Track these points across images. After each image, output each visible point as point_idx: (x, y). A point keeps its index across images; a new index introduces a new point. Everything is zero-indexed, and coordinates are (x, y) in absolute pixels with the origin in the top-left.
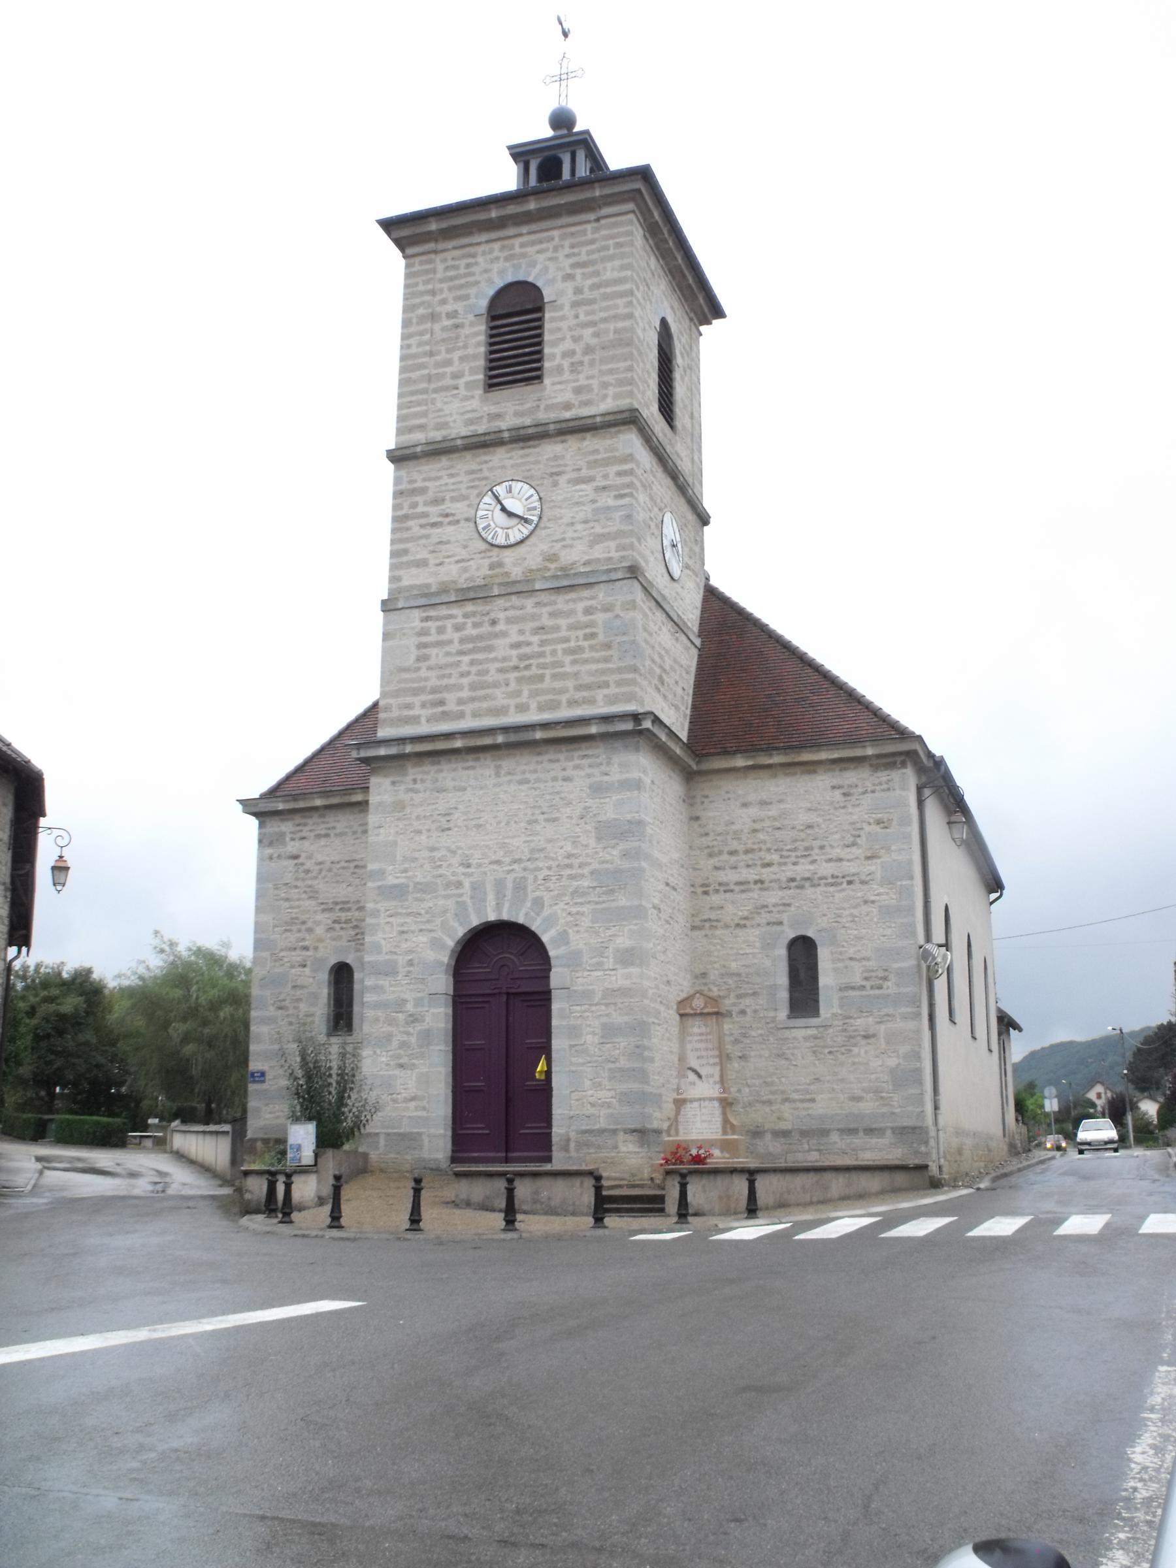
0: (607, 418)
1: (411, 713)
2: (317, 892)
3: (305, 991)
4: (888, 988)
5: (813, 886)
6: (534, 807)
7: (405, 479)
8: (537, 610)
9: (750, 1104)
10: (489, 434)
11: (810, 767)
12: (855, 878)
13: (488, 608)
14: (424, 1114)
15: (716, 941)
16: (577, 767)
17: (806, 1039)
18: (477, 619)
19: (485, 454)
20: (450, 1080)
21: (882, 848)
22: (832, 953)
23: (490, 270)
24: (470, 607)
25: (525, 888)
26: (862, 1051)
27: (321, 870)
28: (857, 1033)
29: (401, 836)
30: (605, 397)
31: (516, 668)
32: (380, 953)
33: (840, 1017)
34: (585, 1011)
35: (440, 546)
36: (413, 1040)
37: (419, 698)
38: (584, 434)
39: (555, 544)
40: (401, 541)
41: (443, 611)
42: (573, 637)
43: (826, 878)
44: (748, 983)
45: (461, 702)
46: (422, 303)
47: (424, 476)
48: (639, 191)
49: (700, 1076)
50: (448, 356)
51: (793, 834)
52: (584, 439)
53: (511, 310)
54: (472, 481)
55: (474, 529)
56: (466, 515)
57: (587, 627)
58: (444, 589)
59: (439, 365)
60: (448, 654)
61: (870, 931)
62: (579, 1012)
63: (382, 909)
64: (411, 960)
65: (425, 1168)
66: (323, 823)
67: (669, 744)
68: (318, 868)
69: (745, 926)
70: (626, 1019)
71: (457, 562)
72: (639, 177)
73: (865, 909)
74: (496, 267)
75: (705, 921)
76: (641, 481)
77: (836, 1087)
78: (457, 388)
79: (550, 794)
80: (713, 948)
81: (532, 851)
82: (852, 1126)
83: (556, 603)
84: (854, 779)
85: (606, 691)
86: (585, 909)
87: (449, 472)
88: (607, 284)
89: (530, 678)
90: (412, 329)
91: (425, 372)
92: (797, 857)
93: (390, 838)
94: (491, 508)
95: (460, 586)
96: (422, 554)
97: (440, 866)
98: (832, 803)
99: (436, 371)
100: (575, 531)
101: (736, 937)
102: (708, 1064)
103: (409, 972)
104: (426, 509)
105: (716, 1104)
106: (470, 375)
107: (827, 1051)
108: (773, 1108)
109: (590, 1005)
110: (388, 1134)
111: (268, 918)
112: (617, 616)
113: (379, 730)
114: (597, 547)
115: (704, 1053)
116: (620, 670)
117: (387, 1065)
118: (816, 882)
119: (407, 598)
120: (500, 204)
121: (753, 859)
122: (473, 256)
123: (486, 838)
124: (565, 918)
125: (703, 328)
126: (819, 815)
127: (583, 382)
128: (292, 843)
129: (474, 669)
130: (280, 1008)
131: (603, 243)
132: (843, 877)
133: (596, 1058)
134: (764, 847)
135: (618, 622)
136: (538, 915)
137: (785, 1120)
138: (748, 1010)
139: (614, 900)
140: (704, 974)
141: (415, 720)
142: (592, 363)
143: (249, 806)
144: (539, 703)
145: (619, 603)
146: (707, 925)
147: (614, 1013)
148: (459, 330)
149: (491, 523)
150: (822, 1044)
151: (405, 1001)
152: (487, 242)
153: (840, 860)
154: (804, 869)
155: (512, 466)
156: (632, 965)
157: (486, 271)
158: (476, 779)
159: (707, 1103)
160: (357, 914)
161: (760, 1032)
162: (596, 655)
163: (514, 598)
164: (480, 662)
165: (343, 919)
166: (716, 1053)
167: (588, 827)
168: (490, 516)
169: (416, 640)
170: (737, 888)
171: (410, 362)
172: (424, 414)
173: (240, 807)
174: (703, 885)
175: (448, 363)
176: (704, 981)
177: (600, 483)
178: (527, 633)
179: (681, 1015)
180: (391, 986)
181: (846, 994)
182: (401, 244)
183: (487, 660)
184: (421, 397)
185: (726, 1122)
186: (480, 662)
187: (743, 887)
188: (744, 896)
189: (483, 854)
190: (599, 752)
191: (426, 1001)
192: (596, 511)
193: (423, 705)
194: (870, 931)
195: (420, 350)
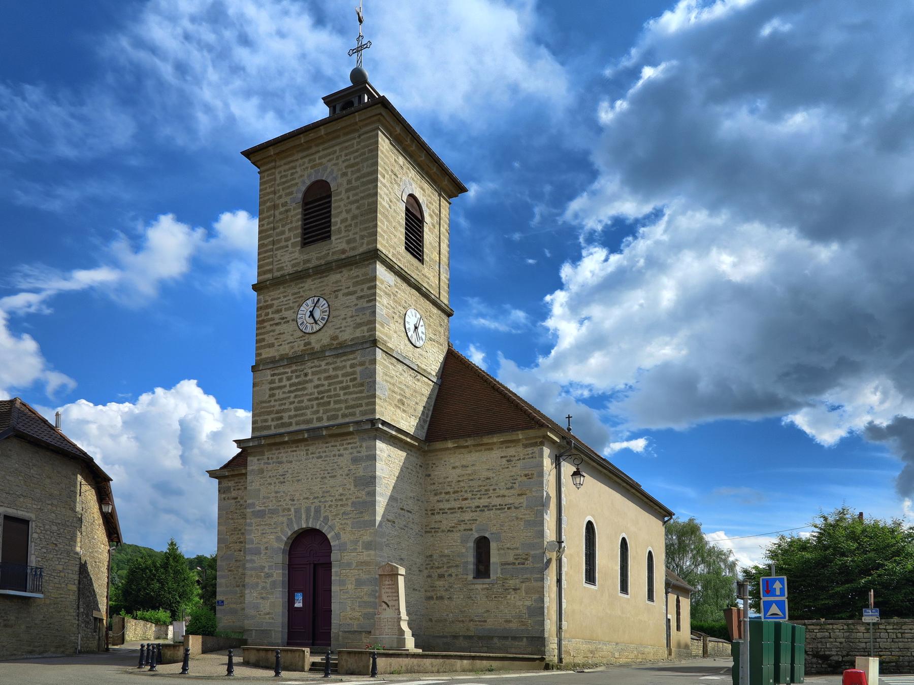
1: (267, 424)
3: (241, 563)
4: (528, 564)
13: (303, 367)
14: (273, 621)
16: (345, 449)
23: (304, 175)
26: (512, 597)
39: (336, 330)
42: (345, 380)
43: (496, 506)
45: (290, 417)
46: (268, 200)
48: (380, 114)
49: (388, 606)
50: (283, 229)
54: (295, 298)
56: (292, 318)
57: (352, 375)
58: (283, 358)
59: (278, 234)
60: (284, 393)
69: (452, 531)
70: (367, 577)
71: (288, 343)
72: (380, 105)
74: (306, 173)
83: (336, 362)
85: (361, 409)
86: (348, 522)
88: (364, 176)
89: (324, 403)
90: (264, 215)
96: (272, 340)
99: (277, 238)
100: (346, 322)
103: (266, 553)
109: (351, 570)
110: (256, 630)
112: (367, 368)
118: (491, 507)
119: (264, 364)
122: (294, 168)
129: (296, 400)
132: (505, 505)
134: (464, 490)
144: (328, 416)
146: (433, 530)
149: (305, 321)
152: (301, 158)
153: (504, 496)
154: (484, 501)
155: (315, 289)
162: (355, 389)
170: (449, 511)
171: (264, 234)
172: (272, 263)
174: (431, 510)
175: (283, 233)
177: (360, 294)
181: (504, 567)
184: (269, 254)
187: (452, 511)
191: (274, 567)
193: (273, 420)
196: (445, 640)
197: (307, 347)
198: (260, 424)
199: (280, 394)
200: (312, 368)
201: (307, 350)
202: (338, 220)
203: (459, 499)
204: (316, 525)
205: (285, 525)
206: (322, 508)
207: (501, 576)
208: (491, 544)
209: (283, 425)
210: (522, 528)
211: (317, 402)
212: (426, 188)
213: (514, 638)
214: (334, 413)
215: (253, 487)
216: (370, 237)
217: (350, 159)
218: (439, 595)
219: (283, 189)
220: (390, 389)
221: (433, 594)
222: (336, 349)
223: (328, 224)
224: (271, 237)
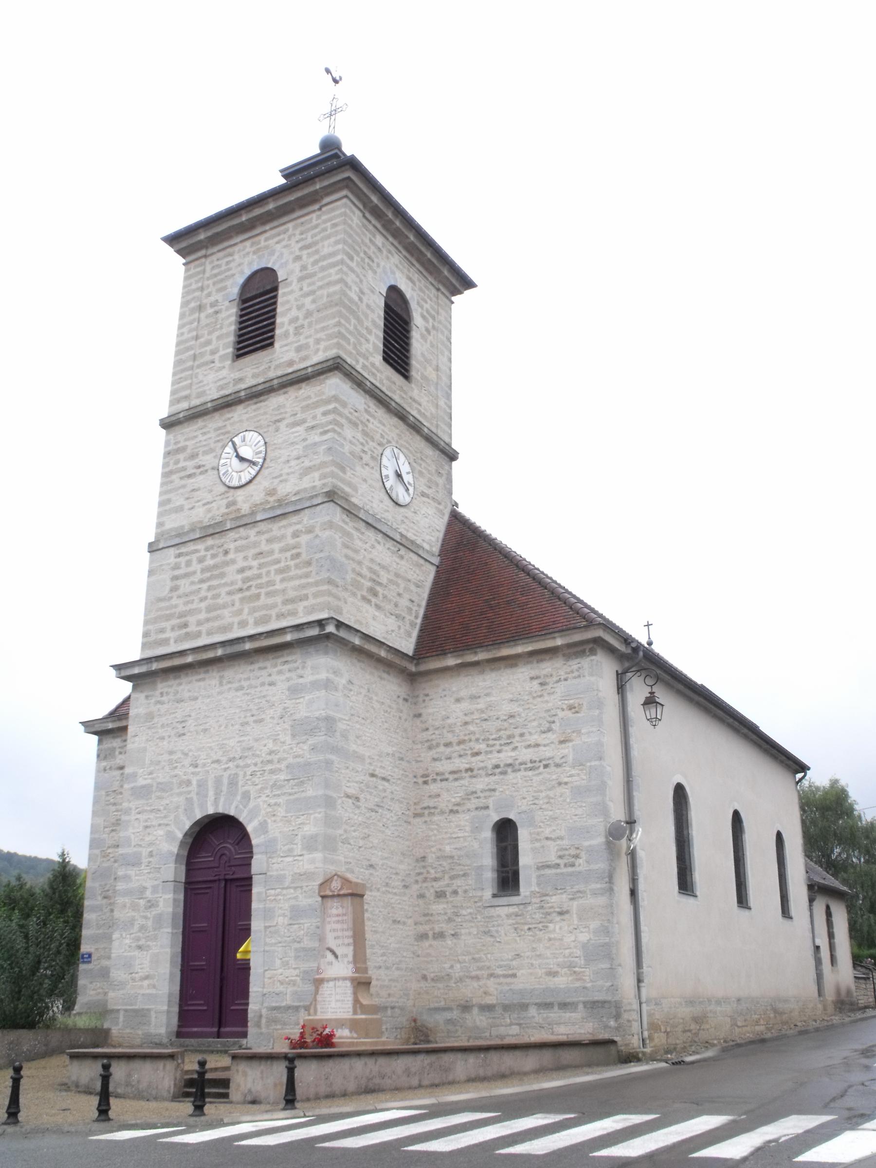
4: (580, 865)
5: (514, 771)
6: (246, 710)
7: (173, 442)
9: (461, 980)
11: (511, 661)
12: (550, 762)
13: (223, 540)
15: (433, 827)
16: (280, 672)
17: (508, 916)
19: (229, 412)
20: (179, 959)
21: (573, 732)
22: (531, 834)
24: (210, 542)
25: (237, 784)
26: (557, 927)
28: (552, 910)
29: (150, 743)
30: (318, 350)
33: (538, 895)
34: (278, 895)
35: (193, 493)
36: (150, 923)
41: (191, 547)
42: (283, 559)
44: (460, 865)
45: (199, 623)
48: (349, 178)
49: (336, 957)
50: (209, 337)
51: (498, 724)
52: (301, 388)
55: (217, 476)
56: (211, 466)
60: (193, 583)
61: (563, 811)
62: (273, 896)
63: (134, 807)
64: (151, 852)
65: (151, 1043)
67: (366, 647)
69: (457, 812)
71: (204, 505)
72: (348, 167)
73: (559, 790)
74: (247, 260)
75: (425, 808)
76: (347, 418)
77: (534, 962)
78: (213, 362)
79: (259, 698)
81: (244, 750)
82: (548, 1001)
83: (271, 530)
84: (550, 670)
85: (305, 603)
86: (280, 800)
88: (324, 258)
89: (250, 597)
91: (192, 352)
92: (501, 745)
94: (229, 456)
97: (176, 768)
98: (530, 693)
99: (200, 351)
100: (290, 467)
101: (450, 822)
102: (343, 944)
103: (150, 862)
108: (481, 983)
109: (283, 889)
110: (126, 1011)
111: (100, 821)
112: (317, 536)
115: (340, 934)
116: (317, 584)
117: (130, 947)
118: (517, 767)
120: (248, 209)
121: (465, 750)
122: (231, 255)
123: (210, 740)
125: (453, 298)
126: (520, 705)
127: (303, 341)
128: (120, 756)
129: (210, 594)
130: (105, 897)
132: (540, 761)
133: (286, 939)
134: (473, 738)
135: (317, 541)
136: (245, 807)
137: (491, 995)
138: (459, 890)
139: (303, 791)
140: (424, 857)
142: (310, 325)
143: (90, 726)
144: (255, 618)
145: (319, 524)
146: (426, 812)
147: (300, 896)
148: (219, 315)
149: (230, 469)
150: (522, 921)
151: (145, 888)
152: (242, 242)
153: (537, 745)
154: (507, 756)
155: (247, 419)
156: (316, 850)
161: (469, 911)
162: (299, 572)
163: (241, 530)
166: (350, 933)
168: (228, 463)
170: (451, 777)
173: (82, 728)
174: (423, 776)
175: (208, 342)
176: (423, 864)
178: (250, 559)
179: (323, 897)
180: (136, 875)
181: (542, 872)
182: (181, 252)
183: (219, 586)
185: (356, 1001)
187: (456, 776)
188: (457, 784)
190: (296, 658)
191: (160, 887)
193: (173, 629)
194: (563, 811)
196: (448, 1015)
198: (153, 638)
200: (235, 541)
201: (231, 513)
204: (230, 808)
206: (241, 778)
209: (188, 636)
211: (240, 595)
212: (416, 280)
213: (564, 1006)
215: (136, 745)
216: (329, 340)
217: (306, 239)
218: (437, 930)
219: (214, 284)
220: (354, 570)
222: (272, 508)
223: (271, 327)
224: (192, 349)
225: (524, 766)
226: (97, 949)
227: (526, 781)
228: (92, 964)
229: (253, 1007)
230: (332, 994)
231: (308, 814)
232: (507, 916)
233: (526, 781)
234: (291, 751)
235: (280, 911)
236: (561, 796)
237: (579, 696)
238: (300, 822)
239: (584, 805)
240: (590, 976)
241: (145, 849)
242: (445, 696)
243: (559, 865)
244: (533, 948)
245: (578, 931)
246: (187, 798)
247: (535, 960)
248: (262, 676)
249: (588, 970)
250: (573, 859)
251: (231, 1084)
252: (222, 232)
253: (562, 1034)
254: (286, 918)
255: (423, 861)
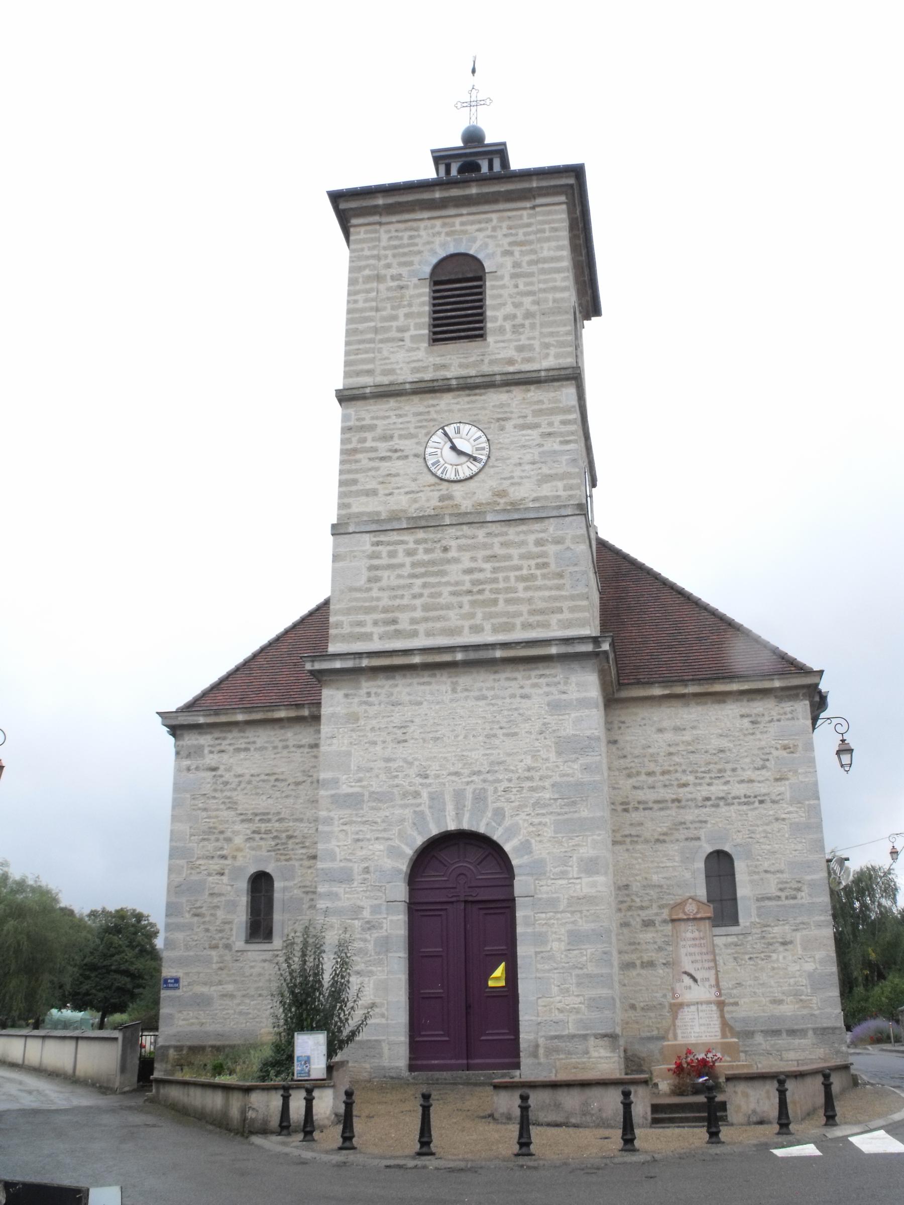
0: (551, 373)
1: (363, 630)
2: (236, 803)
3: (223, 898)
4: (802, 898)
6: (493, 722)
7: (353, 417)
8: (489, 540)
10: (437, 380)
11: (721, 697)
12: (766, 798)
13: (439, 536)
14: (383, 1021)
16: (535, 685)
18: (429, 545)
19: (432, 398)
22: (748, 866)
23: (433, 242)
24: (421, 534)
26: (781, 957)
27: (240, 782)
28: (774, 940)
29: (355, 747)
30: (547, 355)
31: (470, 592)
32: (333, 859)
33: (758, 926)
34: (550, 919)
35: (389, 478)
36: (370, 947)
37: (371, 616)
38: (528, 387)
40: (349, 472)
41: (395, 537)
42: (525, 566)
43: (739, 798)
44: (669, 894)
45: (413, 621)
47: (372, 414)
49: (695, 980)
50: (394, 312)
51: (708, 757)
52: (529, 390)
53: (453, 277)
54: (420, 421)
56: (414, 452)
58: (394, 517)
59: (384, 319)
60: (399, 576)
61: (782, 846)
62: (544, 919)
63: (336, 817)
64: (367, 868)
65: (385, 1077)
66: (242, 737)
68: (237, 780)
69: (664, 841)
70: (593, 926)
71: (407, 493)
72: (573, 174)
73: (776, 826)
74: (437, 240)
75: (626, 836)
77: (757, 991)
78: (403, 341)
79: (509, 710)
80: (634, 862)
82: (774, 1028)
85: (560, 616)
87: (397, 412)
89: (483, 601)
90: (358, 287)
91: (372, 324)
92: (711, 778)
93: (344, 748)
94: (440, 446)
95: (410, 515)
96: (372, 485)
97: (396, 777)
98: (741, 730)
99: (382, 325)
100: (523, 471)
101: (656, 851)
103: (365, 879)
104: (374, 444)
105: (714, 1008)
106: (416, 329)
107: (747, 957)
109: (556, 912)
111: (185, 828)
112: (568, 548)
113: (330, 645)
114: (545, 486)
115: (698, 958)
116: (572, 598)
118: (730, 801)
119: (357, 524)
122: (417, 229)
123: (444, 750)
124: (526, 828)
127: (524, 341)
128: (211, 756)
129: (426, 592)
131: (539, 227)
132: (755, 797)
133: (564, 964)
134: (680, 769)
136: (500, 825)
139: (576, 812)
140: (627, 886)
141: (368, 637)
144: (493, 625)
145: (569, 536)
146: (628, 840)
148: (403, 291)
149: (441, 460)
150: (742, 951)
152: (429, 219)
154: (718, 789)
155: (459, 410)
156: (598, 874)
157: (428, 243)
158: (432, 694)
159: (704, 1007)
160: (277, 825)
163: (465, 527)
164: (433, 585)
165: (263, 830)
167: (548, 742)
168: (439, 453)
169: (366, 563)
170: (656, 806)
171: (357, 315)
172: (372, 360)
174: (622, 804)
175: (394, 318)
176: (626, 892)
178: (480, 561)
180: (345, 893)
181: (763, 904)
183: (439, 584)
184: (368, 346)
186: (433, 585)
187: (661, 806)
188: (662, 813)
189: (440, 766)
190: (557, 672)
191: (384, 908)
192: (542, 454)
193: (376, 623)
194: (782, 846)
195: (367, 305)
197: (446, 503)
199: (392, 578)
200: (457, 538)
202: (500, 314)
203: (671, 785)
204: (478, 825)
205: (407, 825)
207: (757, 920)
208: (736, 864)
210: (787, 836)
211: (469, 598)
213: (792, 1032)
214: (505, 620)
216: (561, 347)
218: (646, 959)
221: (634, 956)
225: (737, 800)
226: (187, 974)
227: (740, 814)
228: (181, 990)
229: (526, 1037)
230: (694, 1018)
231: (583, 836)
232: (725, 945)
233: (740, 814)
234: (557, 769)
235: (554, 935)
236: (779, 832)
237: (793, 737)
238: (573, 843)
239: (804, 841)
240: (817, 1004)
241: (356, 865)
242: (645, 725)
243: (779, 897)
244: (756, 977)
245: (802, 960)
246: (415, 812)
247: (759, 989)
248: (511, 687)
249: (815, 998)
250: (794, 892)
251: (728, 1106)
252: (407, 202)
253: (792, 1060)
254: (563, 943)
255: (626, 889)
